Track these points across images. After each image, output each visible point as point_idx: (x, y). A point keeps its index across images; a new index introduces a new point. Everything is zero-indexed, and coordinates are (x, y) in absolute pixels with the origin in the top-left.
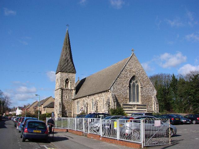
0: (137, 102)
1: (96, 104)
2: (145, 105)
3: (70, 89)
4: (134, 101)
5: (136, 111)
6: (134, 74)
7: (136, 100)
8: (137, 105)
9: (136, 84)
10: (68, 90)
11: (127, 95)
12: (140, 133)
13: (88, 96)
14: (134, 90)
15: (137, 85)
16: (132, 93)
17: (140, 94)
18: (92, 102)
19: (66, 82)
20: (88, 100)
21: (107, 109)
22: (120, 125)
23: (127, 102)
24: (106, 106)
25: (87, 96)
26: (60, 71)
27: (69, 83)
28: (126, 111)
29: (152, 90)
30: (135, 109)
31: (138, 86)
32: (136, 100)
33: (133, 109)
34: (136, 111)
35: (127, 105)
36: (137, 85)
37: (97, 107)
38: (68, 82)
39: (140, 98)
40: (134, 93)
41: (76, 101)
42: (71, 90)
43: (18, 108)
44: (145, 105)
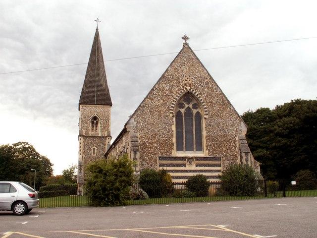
2: (219, 159)
3: (100, 135)
4: (190, 149)
5: (194, 171)
6: (188, 88)
7: (195, 146)
8: (197, 159)
9: (195, 111)
10: (89, 137)
11: (170, 138)
15: (198, 112)
16: (194, 122)
17: (204, 133)
19: (93, 123)
23: (170, 152)
27: (99, 125)
29: (239, 125)
30: (193, 167)
31: (199, 116)
32: (195, 146)
33: (188, 168)
34: (194, 171)
35: (171, 158)
36: (198, 112)
38: (97, 123)
40: (189, 132)
42: (103, 137)
43: (212, 189)
44: (219, 159)
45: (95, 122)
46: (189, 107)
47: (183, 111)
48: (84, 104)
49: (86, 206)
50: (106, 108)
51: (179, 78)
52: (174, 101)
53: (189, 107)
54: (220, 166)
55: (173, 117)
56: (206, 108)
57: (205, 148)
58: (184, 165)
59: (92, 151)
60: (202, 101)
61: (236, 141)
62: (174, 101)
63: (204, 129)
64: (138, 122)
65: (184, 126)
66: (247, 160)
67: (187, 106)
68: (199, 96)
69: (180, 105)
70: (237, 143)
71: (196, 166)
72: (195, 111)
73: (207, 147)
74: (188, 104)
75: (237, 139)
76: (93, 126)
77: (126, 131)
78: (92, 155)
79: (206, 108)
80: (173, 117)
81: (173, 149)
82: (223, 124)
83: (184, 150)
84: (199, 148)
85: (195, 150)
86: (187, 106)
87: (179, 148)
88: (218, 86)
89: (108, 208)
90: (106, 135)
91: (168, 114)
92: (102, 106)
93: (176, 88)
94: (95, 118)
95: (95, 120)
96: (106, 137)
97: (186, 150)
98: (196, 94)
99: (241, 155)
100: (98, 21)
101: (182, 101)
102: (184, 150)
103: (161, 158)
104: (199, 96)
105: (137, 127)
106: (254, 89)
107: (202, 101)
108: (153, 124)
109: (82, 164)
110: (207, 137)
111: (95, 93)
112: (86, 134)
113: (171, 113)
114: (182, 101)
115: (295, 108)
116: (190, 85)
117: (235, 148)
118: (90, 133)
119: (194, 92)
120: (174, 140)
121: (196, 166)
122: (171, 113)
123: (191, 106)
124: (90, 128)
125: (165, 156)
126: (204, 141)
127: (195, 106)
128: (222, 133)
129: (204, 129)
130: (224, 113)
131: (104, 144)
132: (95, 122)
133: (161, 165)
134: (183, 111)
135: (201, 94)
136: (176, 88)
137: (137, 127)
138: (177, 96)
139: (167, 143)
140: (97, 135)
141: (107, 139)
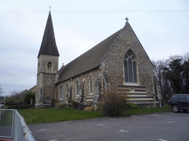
0: (125, 82)
1: (82, 87)
3: (52, 73)
4: (131, 81)
8: (136, 87)
9: (133, 60)
10: (46, 73)
11: (122, 75)
12: (150, 113)
13: (72, 78)
14: (130, 68)
15: (134, 61)
16: (133, 67)
17: (138, 73)
18: (77, 85)
19: (48, 65)
20: (72, 84)
21: (98, 92)
22: (35, 123)
24: (96, 88)
25: (70, 78)
26: (42, 54)
27: (52, 67)
28: (145, 94)
31: (135, 63)
32: (133, 80)
33: (131, 92)
35: (123, 86)
37: (83, 91)
38: (51, 66)
39: (138, 78)
40: (131, 72)
41: (59, 86)
44: (145, 87)
45: (50, 65)
46: (130, 58)
47: (127, 60)
48: (43, 54)
49: (100, 116)
50: (55, 57)
51: (125, 41)
52: (123, 54)
53: (130, 58)
54: (145, 91)
55: (123, 63)
56: (138, 59)
57: (138, 81)
58: (129, 91)
59: (48, 82)
60: (136, 55)
61: (152, 78)
62: (123, 54)
63: (138, 71)
64: (106, 65)
65: (128, 69)
66: (108, 86)
67: (129, 57)
68: (135, 52)
69: (126, 57)
70: (152, 79)
71: (135, 91)
72: (133, 60)
73: (139, 80)
74: (129, 56)
75: (152, 77)
76: (48, 67)
77: (99, 69)
78: (48, 84)
79: (138, 59)
80: (123, 63)
81: (123, 81)
82: (146, 68)
83: (129, 82)
84: (136, 81)
85: (133, 82)
86: (129, 57)
87: (126, 81)
88: (143, 48)
89: (107, 118)
90: (56, 73)
91: (121, 61)
92: (46, 55)
93: (124, 47)
94: (50, 63)
95: (50, 64)
96: (56, 74)
97: (130, 82)
98: (133, 51)
99: (155, 85)
100: (50, 7)
101: (127, 54)
102: (129, 82)
103: (119, 86)
104: (135, 52)
105: (106, 67)
106: (160, 51)
107: (136, 55)
108: (114, 66)
109: (42, 89)
110: (139, 75)
111: (49, 47)
112: (44, 71)
113: (122, 60)
114: (127, 54)
115: (175, 63)
116: (130, 46)
117: (152, 82)
118: (47, 71)
119: (132, 50)
120: (124, 76)
121: (135, 91)
122: (122, 60)
123: (131, 57)
124: (47, 68)
125: (120, 85)
126: (138, 77)
127: (133, 58)
128: (145, 73)
129: (138, 71)
130: (146, 63)
131: (55, 78)
132: (50, 65)
133: (119, 90)
134: (127, 60)
135: (135, 51)
136: (124, 47)
137: (106, 67)
138: (125, 51)
139: (120, 77)
140: (51, 73)
141: (57, 75)
